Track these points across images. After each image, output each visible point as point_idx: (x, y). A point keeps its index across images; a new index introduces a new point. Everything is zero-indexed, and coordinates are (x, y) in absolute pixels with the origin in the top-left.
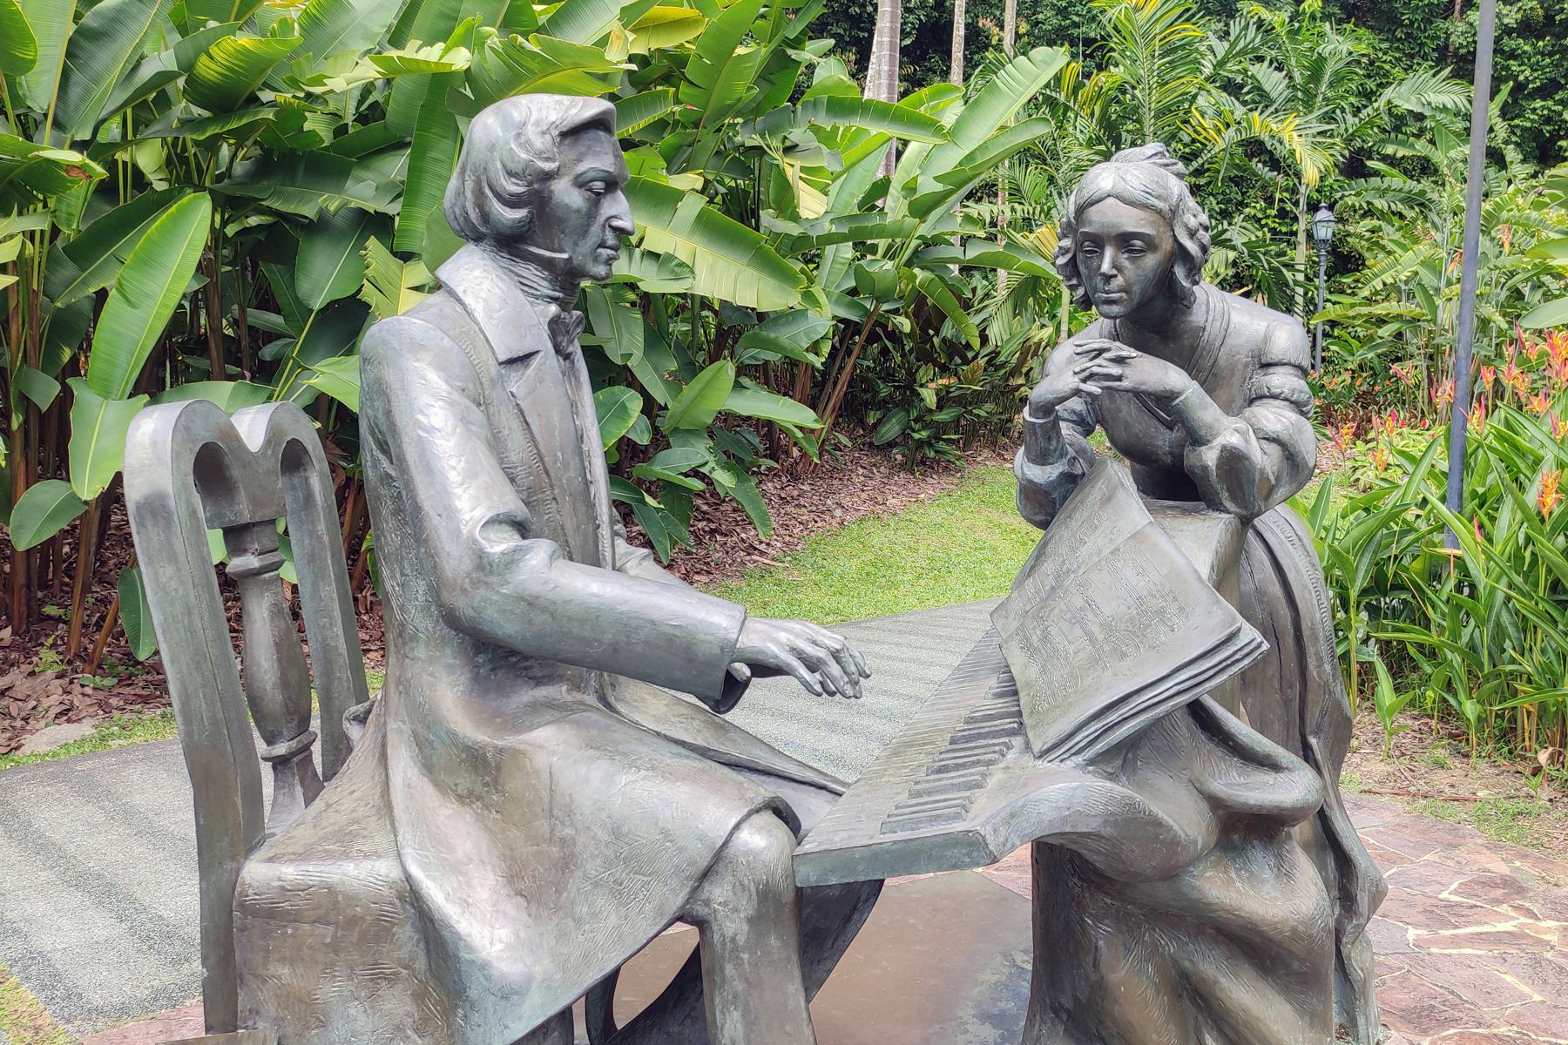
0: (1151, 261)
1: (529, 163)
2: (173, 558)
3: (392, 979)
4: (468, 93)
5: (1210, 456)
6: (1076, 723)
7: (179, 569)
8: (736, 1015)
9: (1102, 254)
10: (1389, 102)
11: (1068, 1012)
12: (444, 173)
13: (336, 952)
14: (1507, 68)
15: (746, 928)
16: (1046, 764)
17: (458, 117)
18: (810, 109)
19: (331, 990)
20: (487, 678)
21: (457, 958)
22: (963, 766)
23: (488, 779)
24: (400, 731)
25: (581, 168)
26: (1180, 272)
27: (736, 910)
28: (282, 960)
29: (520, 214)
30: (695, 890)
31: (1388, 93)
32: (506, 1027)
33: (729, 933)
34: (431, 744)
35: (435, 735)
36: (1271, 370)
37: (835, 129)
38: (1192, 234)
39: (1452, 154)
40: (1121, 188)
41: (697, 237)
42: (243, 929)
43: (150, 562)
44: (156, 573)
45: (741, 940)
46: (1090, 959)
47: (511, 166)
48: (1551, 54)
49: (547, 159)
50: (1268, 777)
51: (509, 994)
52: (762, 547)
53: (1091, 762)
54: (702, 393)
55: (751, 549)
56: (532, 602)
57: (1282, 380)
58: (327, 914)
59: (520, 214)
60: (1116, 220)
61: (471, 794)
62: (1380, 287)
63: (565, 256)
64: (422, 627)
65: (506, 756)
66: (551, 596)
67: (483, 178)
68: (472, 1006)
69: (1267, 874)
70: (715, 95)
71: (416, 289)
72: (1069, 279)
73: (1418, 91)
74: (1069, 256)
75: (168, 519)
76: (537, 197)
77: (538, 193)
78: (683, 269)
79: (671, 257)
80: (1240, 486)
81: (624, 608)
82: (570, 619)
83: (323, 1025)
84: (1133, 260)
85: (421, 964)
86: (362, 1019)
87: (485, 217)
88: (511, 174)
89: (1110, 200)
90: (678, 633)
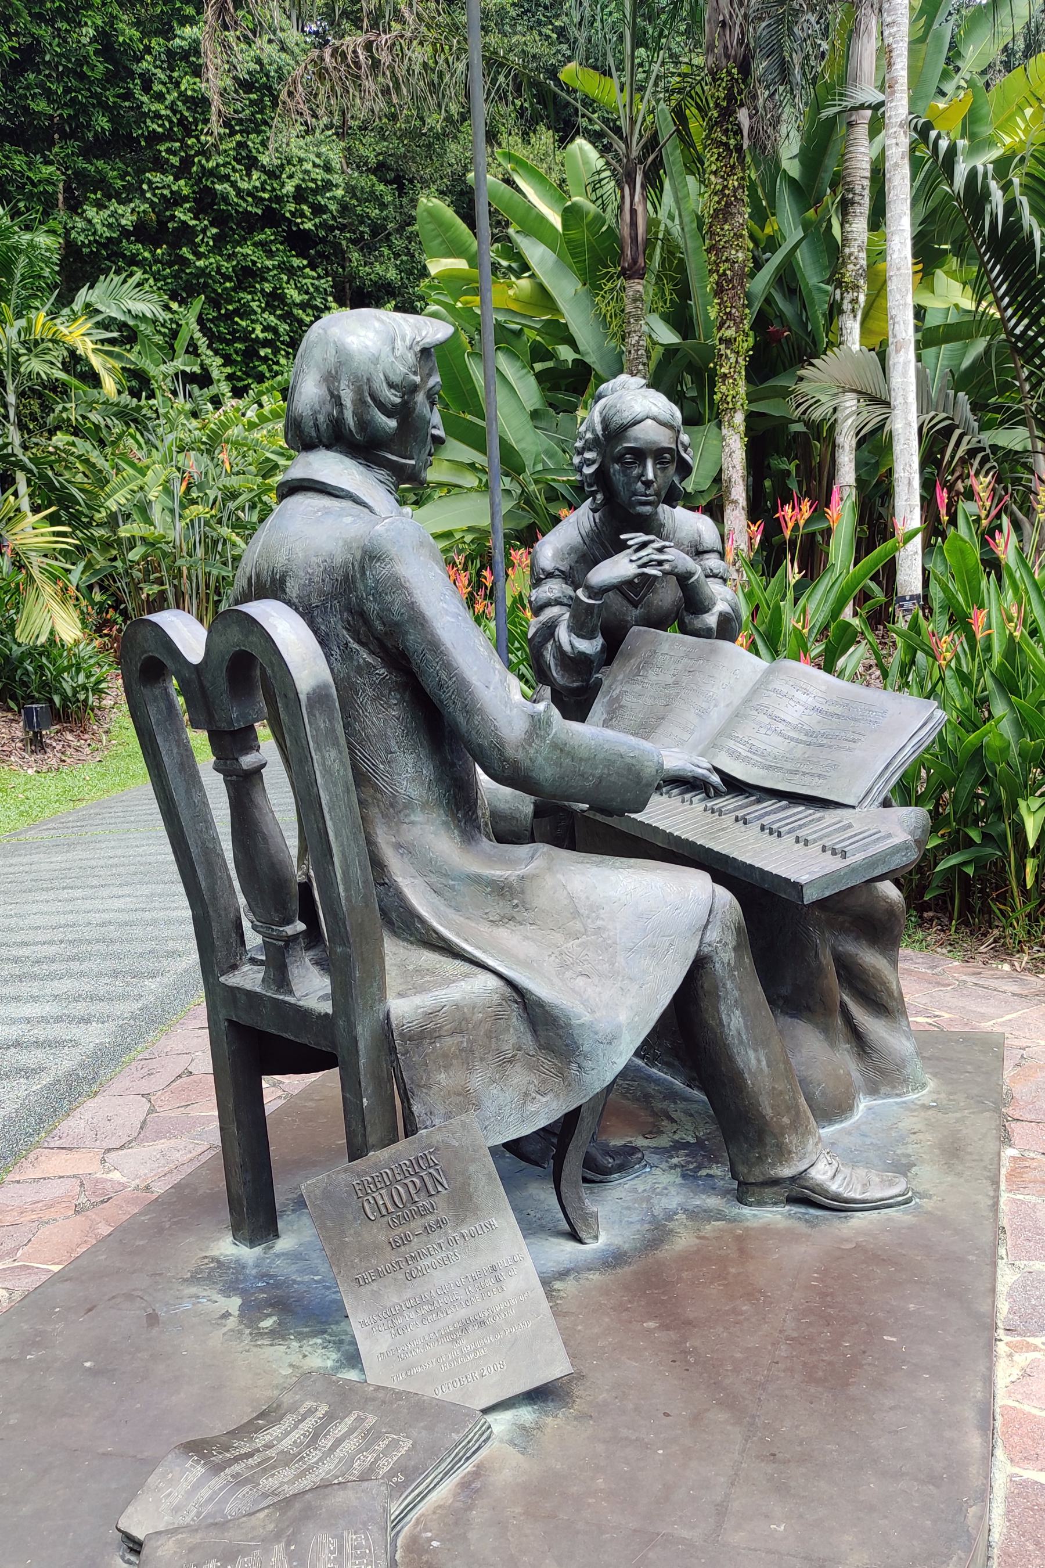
2: (336, 743)
7: (340, 752)
8: (738, 1013)
9: (645, 467)
19: (477, 1080)
21: (569, 1025)
23: (516, 901)
29: (393, 423)
34: (452, 888)
36: (706, 556)
43: (318, 749)
44: (323, 757)
45: (732, 962)
46: (813, 954)
51: (611, 1040)
63: (413, 462)
68: (585, 1057)
74: (595, 467)
85: (528, 1041)
87: (364, 423)
88: (391, 385)
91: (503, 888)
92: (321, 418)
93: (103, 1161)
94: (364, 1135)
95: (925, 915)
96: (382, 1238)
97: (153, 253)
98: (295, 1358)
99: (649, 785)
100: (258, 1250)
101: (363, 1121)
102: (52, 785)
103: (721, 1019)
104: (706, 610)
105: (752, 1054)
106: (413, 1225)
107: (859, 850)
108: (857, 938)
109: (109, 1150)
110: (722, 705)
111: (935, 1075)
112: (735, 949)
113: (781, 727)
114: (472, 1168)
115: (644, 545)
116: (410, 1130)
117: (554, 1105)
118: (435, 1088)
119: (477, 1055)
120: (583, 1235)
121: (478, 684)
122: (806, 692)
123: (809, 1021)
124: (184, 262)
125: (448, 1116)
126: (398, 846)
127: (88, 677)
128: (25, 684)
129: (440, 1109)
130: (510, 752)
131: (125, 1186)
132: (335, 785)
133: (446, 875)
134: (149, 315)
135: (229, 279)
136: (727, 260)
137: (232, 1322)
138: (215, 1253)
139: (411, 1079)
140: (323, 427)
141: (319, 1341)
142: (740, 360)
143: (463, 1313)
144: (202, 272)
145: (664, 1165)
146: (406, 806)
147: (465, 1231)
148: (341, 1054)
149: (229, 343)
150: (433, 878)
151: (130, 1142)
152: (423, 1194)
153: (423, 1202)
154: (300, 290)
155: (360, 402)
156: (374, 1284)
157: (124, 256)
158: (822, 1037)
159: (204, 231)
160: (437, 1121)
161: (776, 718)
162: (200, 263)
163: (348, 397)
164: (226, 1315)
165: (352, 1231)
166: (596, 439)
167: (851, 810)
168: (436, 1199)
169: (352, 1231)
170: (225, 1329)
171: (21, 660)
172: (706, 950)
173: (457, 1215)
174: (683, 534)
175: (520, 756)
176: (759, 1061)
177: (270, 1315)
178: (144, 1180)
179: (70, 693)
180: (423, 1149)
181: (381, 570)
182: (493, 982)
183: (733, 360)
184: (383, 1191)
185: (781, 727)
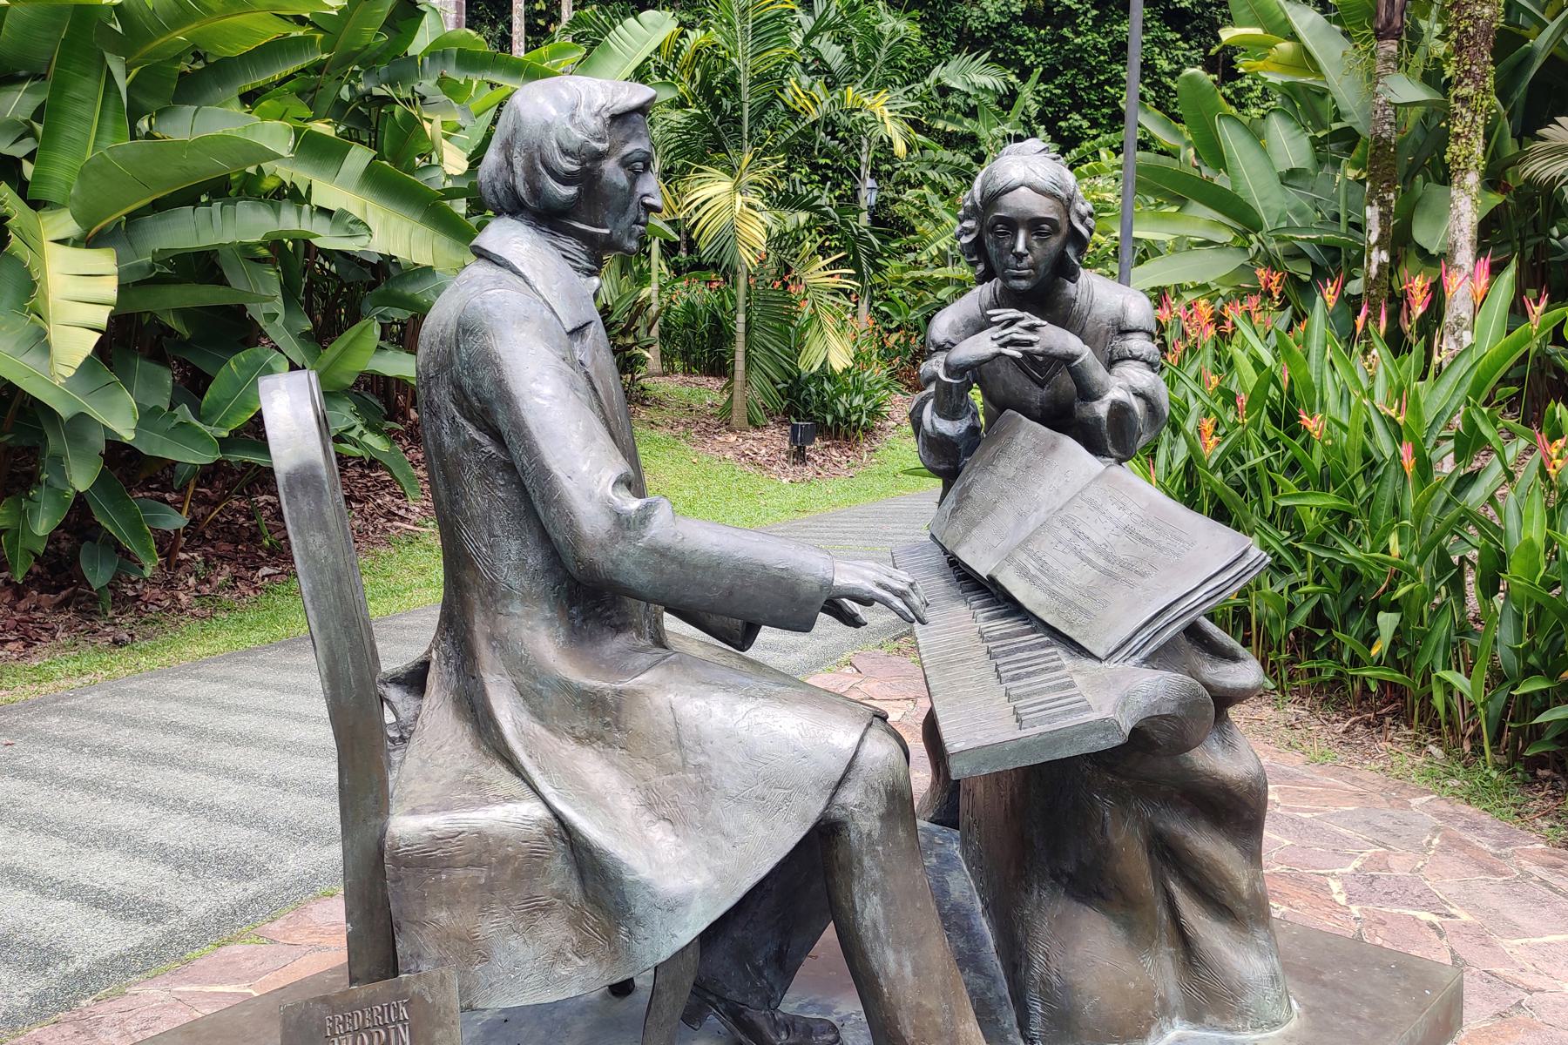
0: (1054, 242)
1: (584, 144)
2: (324, 527)
3: (547, 909)
4: (119, 28)
5: (1102, 409)
6: (1132, 630)
7: (329, 538)
8: (876, 899)
9: (1016, 237)
10: (939, 80)
11: (1070, 876)
12: (85, 114)
13: (491, 891)
14: (1015, 52)
15: (878, 824)
16: (1120, 666)
17: (107, 55)
18: (439, 61)
19: (488, 927)
20: (580, 628)
21: (619, 881)
22: (1028, 675)
24: (500, 684)
25: (627, 149)
26: (1071, 252)
27: (869, 810)
28: (440, 905)
29: (571, 191)
30: (833, 795)
31: (937, 72)
32: (674, 936)
33: (865, 830)
34: (539, 693)
35: (542, 684)
36: (1130, 336)
37: (468, 83)
38: (1082, 220)
39: (994, 131)
40: (1032, 178)
41: (366, 192)
42: (397, 880)
43: (300, 531)
44: (305, 542)
45: (876, 835)
46: (1098, 828)
47: (566, 144)
48: (1051, 42)
49: (600, 140)
50: (1232, 667)
51: (673, 906)
52: (402, 512)
53: (1145, 661)
54: (343, 354)
55: (390, 515)
56: (662, 553)
57: (1138, 344)
58: (480, 856)
59: (571, 191)
60: (1029, 207)
61: (590, 735)
62: (935, 253)
63: (607, 231)
64: (516, 584)
65: (625, 698)
66: (679, 547)
67: (537, 155)
68: (638, 923)
69: (1216, 747)
70: (341, 41)
71: (62, 241)
72: (970, 256)
73: (962, 71)
74: (973, 236)
75: (319, 491)
76: (587, 175)
77: (589, 170)
78: (358, 226)
79: (344, 214)
80: (1123, 434)
81: (741, 555)
82: (695, 567)
83: (486, 958)
84: (1041, 242)
85: (575, 891)
86: (523, 950)
87: (536, 192)
88: (566, 152)
89: (1023, 189)
90: (784, 574)
91: (594, 701)
92: (498, 185)
95: (1540, 772)
97: (1037, 33)
99: (810, 602)
102: (796, 494)
103: (853, 902)
104: (1097, 397)
105: (890, 956)
107: (1041, 721)
108: (1192, 816)
110: (1043, 510)
111: (1310, 1011)
112: (882, 818)
113: (1082, 545)
115: (1012, 322)
121: (559, 473)
122: (1123, 508)
123: (1104, 911)
124: (1065, 39)
126: (491, 638)
127: (865, 400)
128: (807, 403)
130: (585, 552)
132: (321, 572)
133: (535, 678)
134: (991, 87)
135: (1104, 53)
136: (1470, 17)
140: (501, 195)
142: (1478, 119)
144: (1080, 48)
146: (505, 596)
149: (1097, 108)
150: (522, 679)
154: (1170, 60)
155: (531, 170)
157: (1011, 37)
158: (1121, 934)
159: (1085, 13)
160: (424, 968)
161: (1078, 534)
162: (1078, 41)
163: (519, 163)
166: (974, 206)
167: (1097, 664)
171: (807, 382)
172: (837, 813)
174: (1103, 311)
175: (599, 557)
176: (900, 965)
179: (842, 413)
181: (473, 345)
182: (540, 812)
183: (1469, 119)
185: (1082, 545)
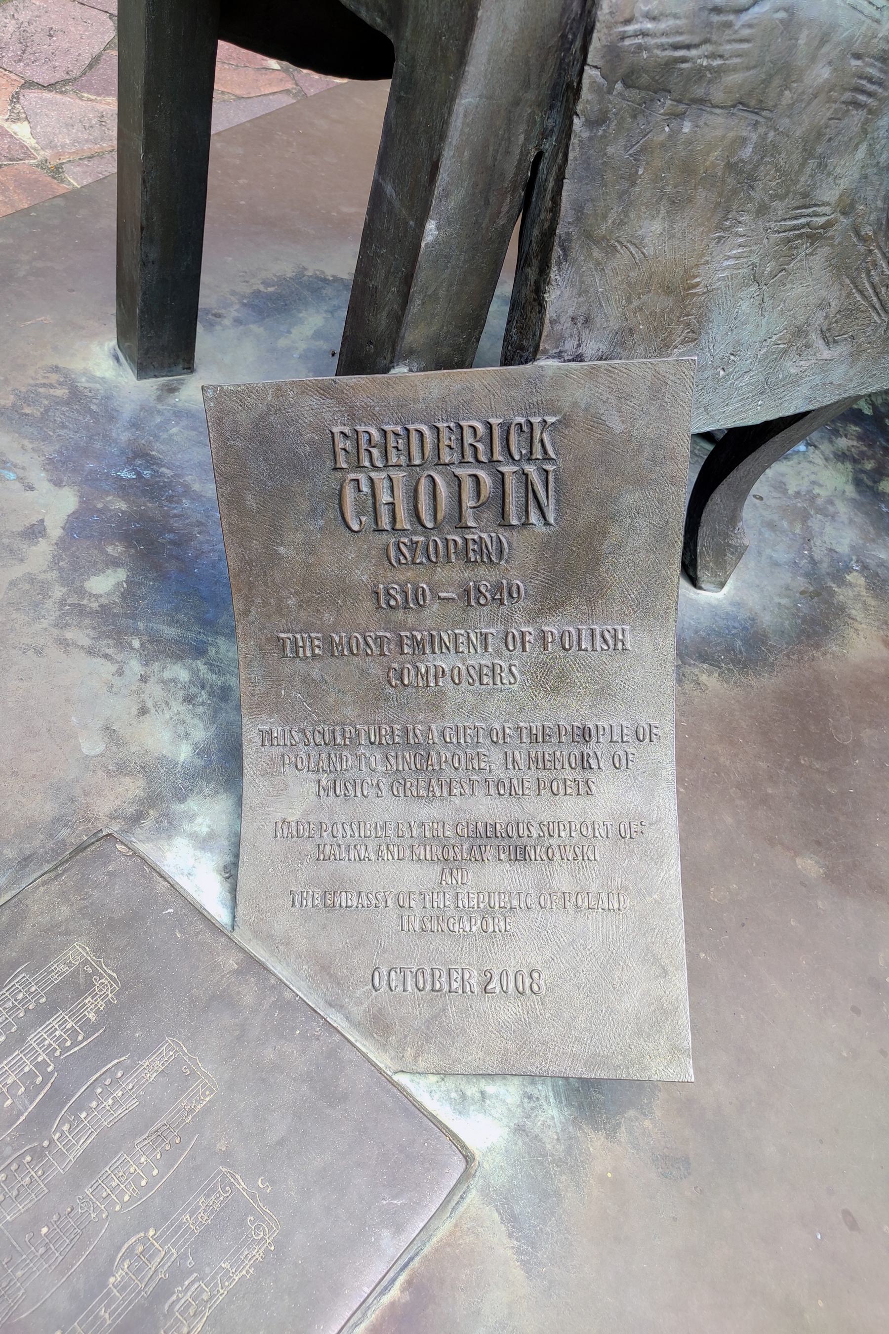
19: (725, 263)
93: (15, 98)
94: (398, 319)
96: (362, 575)
98: (120, 709)
100: (151, 385)
101: (408, 280)
106: (441, 574)
109: (29, 84)
114: (630, 498)
116: (520, 348)
117: (838, 374)
118: (623, 257)
119: (757, 194)
120: (703, 574)
125: (622, 342)
129: (611, 316)
131: (27, 153)
137: (40, 554)
138: (76, 365)
139: (579, 209)
141: (184, 675)
143: (486, 808)
145: (826, 447)
147: (552, 628)
148: (410, 46)
151: (65, 82)
152: (489, 515)
153: (482, 532)
156: (317, 665)
164: (35, 532)
165: (299, 537)
168: (516, 537)
169: (299, 537)
170: (18, 571)
173: (547, 590)
177: (115, 563)
178: (59, 155)
180: (530, 409)
184: (398, 475)
